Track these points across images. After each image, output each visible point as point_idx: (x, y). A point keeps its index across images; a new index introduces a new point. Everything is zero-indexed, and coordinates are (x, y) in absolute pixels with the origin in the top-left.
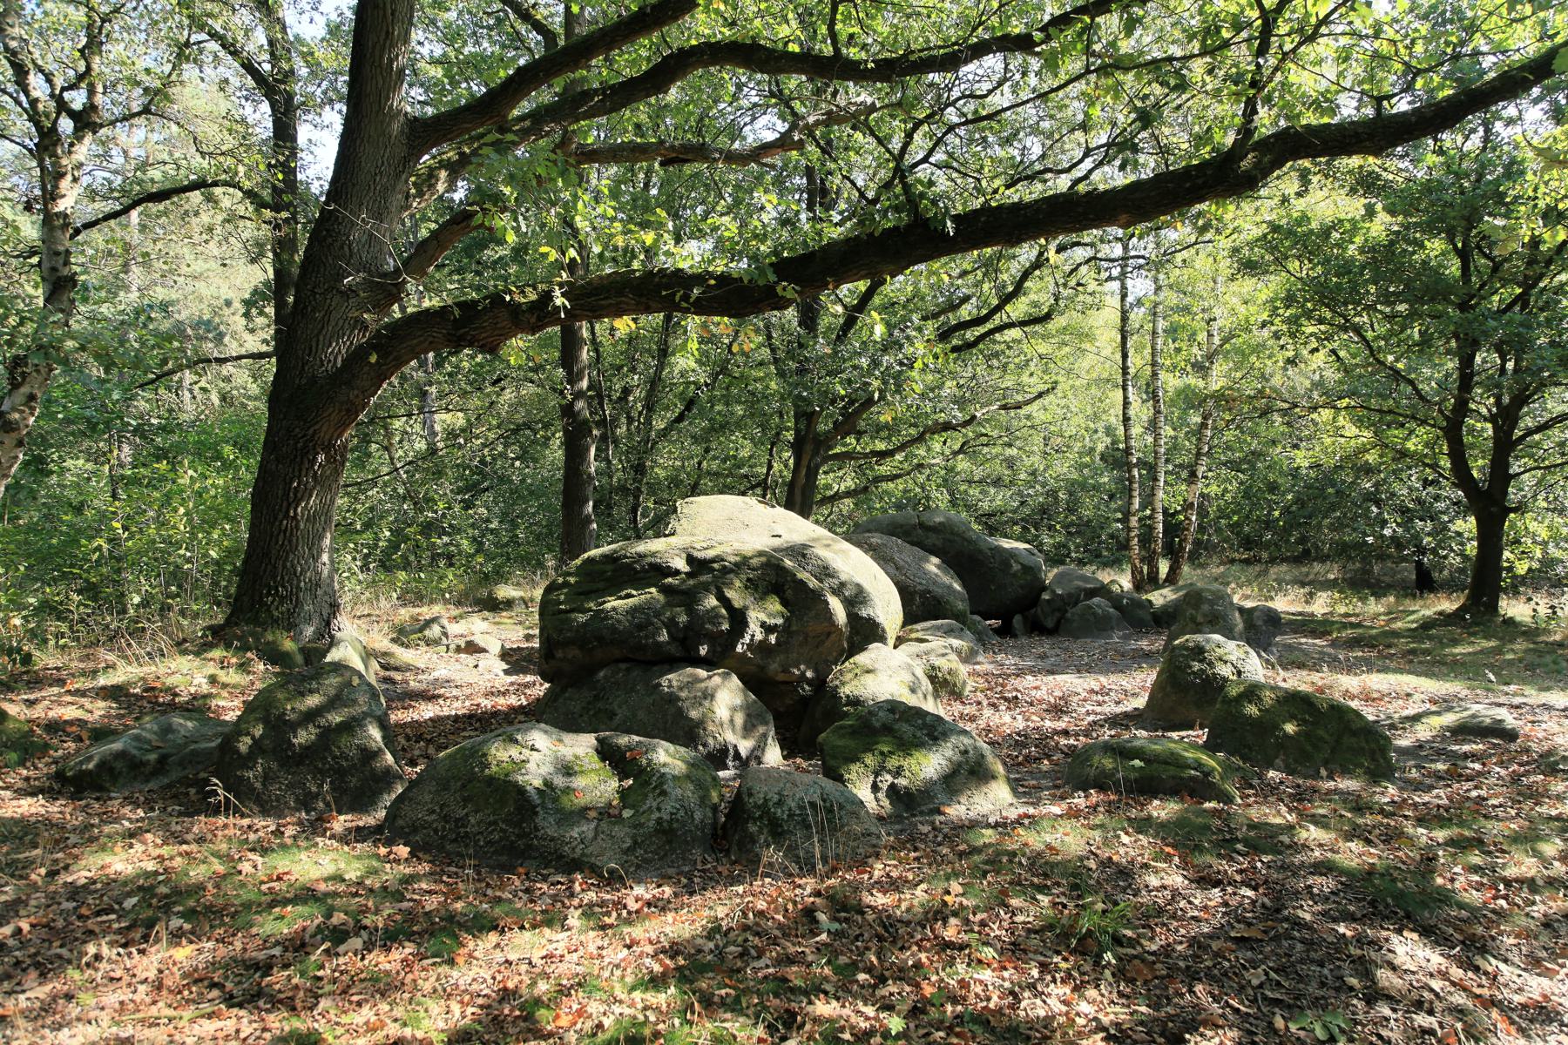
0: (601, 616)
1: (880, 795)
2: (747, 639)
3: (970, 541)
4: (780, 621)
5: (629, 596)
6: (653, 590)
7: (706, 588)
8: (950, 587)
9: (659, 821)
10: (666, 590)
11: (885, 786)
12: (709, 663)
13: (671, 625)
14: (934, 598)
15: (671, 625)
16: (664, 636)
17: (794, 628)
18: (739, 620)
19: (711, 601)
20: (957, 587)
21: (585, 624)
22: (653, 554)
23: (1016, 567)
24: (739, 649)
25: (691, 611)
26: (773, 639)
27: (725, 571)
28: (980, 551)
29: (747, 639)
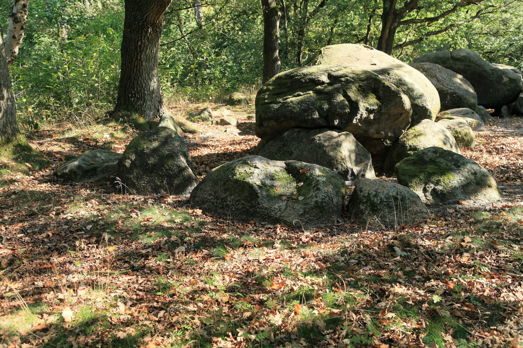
0: (285, 105)
1: (427, 194)
2: (359, 116)
3: (479, 66)
4: (376, 107)
5: (299, 95)
6: (311, 92)
7: (337, 91)
8: (467, 91)
9: (316, 202)
10: (317, 92)
11: (430, 190)
12: (338, 129)
13: (320, 110)
14: (458, 96)
15: (320, 110)
16: (316, 115)
17: (383, 111)
18: (354, 107)
19: (340, 98)
20: (471, 90)
21: (278, 110)
22: (311, 74)
23: (505, 79)
24: (354, 121)
25: (330, 103)
26: (372, 116)
27: (347, 82)
28: (485, 71)
29: (359, 116)
